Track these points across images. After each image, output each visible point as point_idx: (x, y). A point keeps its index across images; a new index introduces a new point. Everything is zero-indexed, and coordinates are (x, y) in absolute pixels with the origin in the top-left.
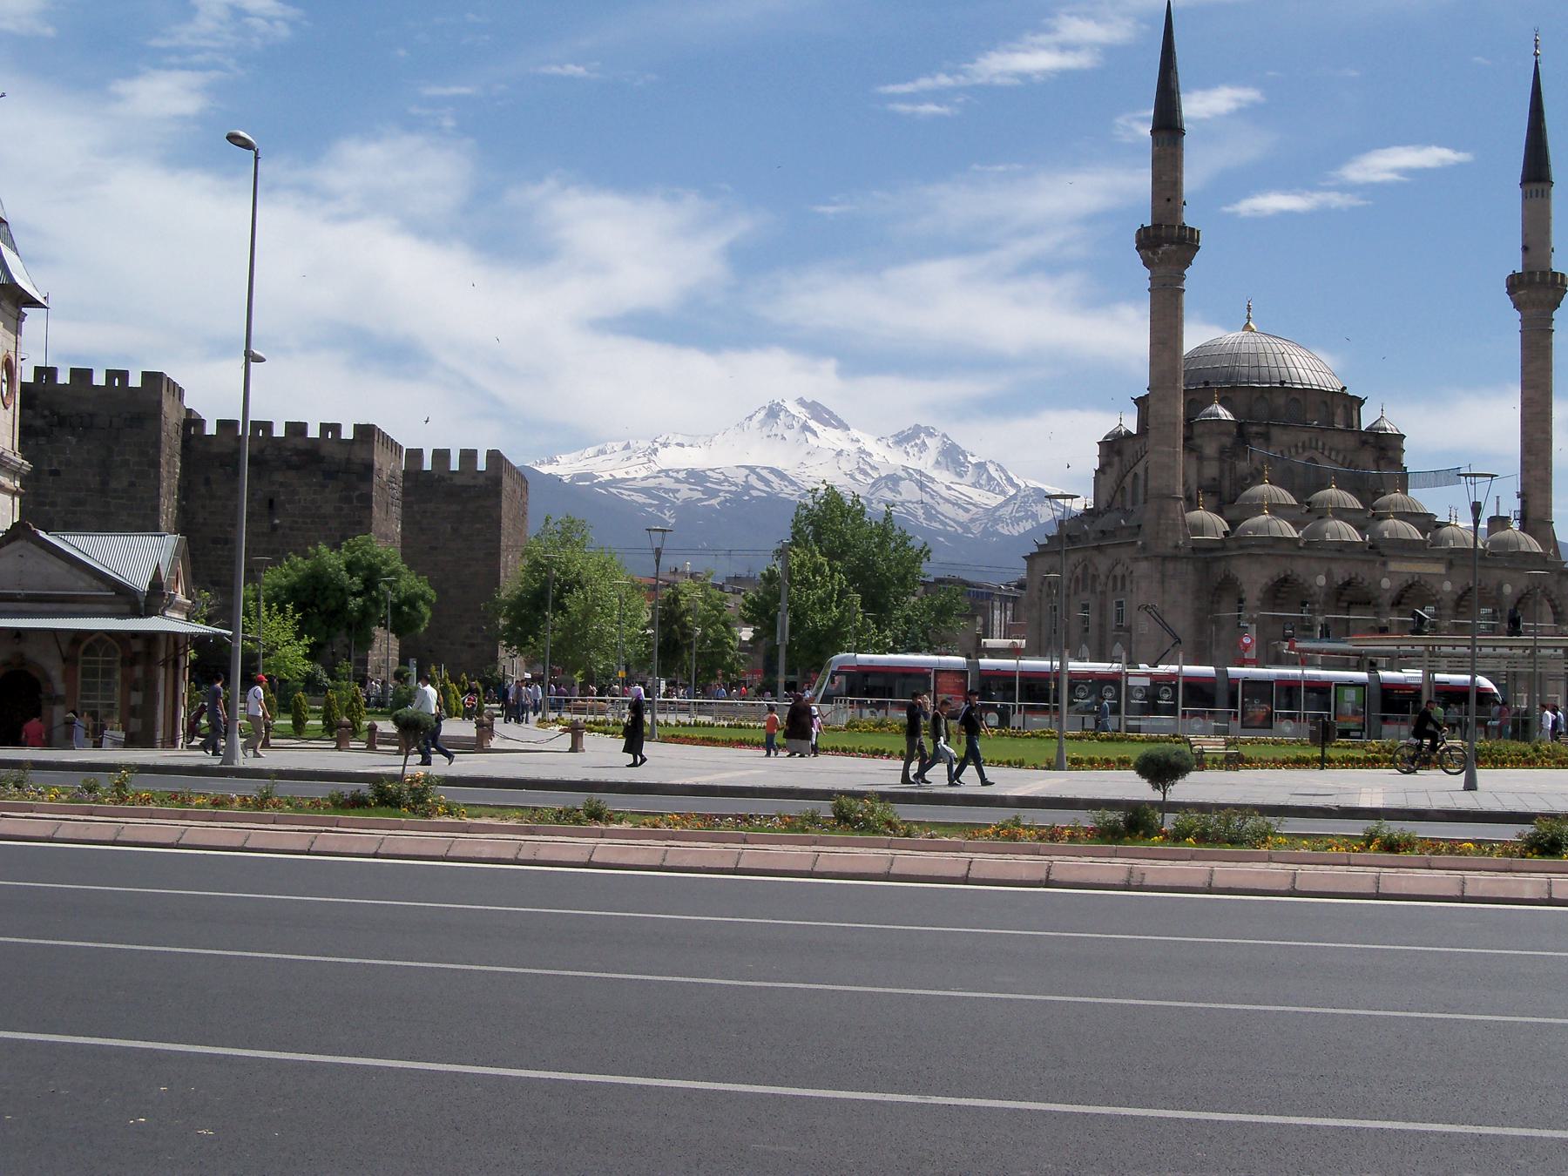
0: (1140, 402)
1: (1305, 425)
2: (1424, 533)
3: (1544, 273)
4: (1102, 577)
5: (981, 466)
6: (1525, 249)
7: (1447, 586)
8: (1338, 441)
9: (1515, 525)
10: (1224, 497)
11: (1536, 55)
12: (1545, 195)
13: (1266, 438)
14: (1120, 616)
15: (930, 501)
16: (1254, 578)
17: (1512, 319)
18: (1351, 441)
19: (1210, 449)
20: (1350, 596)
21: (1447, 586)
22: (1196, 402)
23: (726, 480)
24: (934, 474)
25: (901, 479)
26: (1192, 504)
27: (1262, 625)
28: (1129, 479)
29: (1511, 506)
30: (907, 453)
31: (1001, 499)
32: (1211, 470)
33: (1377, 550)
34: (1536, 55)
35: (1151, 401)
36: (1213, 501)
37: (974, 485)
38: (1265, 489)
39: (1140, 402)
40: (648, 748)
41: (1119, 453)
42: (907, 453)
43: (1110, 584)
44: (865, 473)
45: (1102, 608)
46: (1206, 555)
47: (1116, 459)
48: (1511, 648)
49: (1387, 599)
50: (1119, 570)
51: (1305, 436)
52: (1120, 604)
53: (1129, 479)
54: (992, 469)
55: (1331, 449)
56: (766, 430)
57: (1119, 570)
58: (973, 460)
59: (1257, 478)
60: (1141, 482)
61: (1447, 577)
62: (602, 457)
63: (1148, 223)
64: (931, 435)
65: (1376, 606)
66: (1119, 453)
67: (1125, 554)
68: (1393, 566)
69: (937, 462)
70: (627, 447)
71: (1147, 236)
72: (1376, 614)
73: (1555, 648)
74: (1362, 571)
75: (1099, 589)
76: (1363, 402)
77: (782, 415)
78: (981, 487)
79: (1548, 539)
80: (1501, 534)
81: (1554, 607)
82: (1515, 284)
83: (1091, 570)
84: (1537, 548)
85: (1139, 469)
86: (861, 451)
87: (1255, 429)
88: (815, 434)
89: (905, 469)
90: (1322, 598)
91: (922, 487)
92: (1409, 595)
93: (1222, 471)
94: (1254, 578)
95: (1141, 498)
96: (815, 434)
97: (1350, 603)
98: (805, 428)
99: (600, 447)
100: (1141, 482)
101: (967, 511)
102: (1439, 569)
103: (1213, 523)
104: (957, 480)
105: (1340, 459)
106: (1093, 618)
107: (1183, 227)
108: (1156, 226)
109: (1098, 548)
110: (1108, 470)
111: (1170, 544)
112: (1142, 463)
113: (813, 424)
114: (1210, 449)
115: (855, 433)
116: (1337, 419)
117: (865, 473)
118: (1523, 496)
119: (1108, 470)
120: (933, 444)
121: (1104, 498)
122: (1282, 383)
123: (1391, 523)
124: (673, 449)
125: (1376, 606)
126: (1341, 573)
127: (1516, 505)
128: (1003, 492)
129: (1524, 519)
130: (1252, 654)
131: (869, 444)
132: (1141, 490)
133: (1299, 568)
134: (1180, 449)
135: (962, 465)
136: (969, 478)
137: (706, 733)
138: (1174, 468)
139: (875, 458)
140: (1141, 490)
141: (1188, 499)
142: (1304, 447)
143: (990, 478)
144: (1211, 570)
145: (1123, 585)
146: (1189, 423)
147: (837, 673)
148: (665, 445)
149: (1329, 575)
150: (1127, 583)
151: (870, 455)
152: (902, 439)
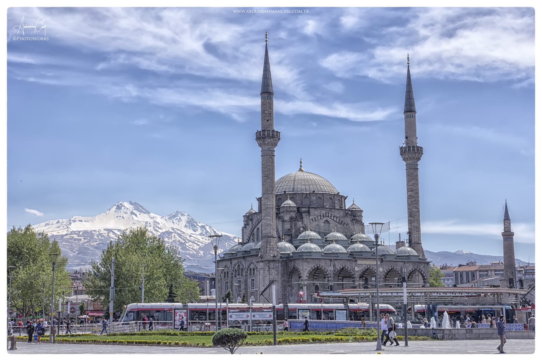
0: (259, 200)
1: (323, 207)
2: (371, 248)
3: (414, 147)
6: (407, 138)
7: (381, 269)
8: (336, 213)
9: (407, 245)
10: (292, 237)
11: (408, 63)
12: (413, 117)
13: (308, 212)
16: (305, 269)
17: (258, 150)
18: (342, 213)
19: (287, 218)
20: (344, 274)
21: (381, 269)
22: (280, 199)
24: (184, 230)
25: (172, 233)
26: (280, 239)
27: (308, 286)
28: (255, 230)
29: (405, 238)
30: (173, 222)
32: (287, 226)
33: (354, 256)
34: (266, 41)
35: (262, 199)
36: (288, 238)
37: (200, 234)
38: (308, 232)
39: (259, 200)
40: (409, 342)
41: (252, 220)
42: (173, 222)
44: (157, 231)
45: (246, 281)
46: (287, 261)
47: (250, 222)
48: (387, 293)
49: (357, 275)
50: (252, 266)
51: (324, 212)
54: (207, 228)
55: (334, 217)
56: (116, 214)
57: (252, 266)
58: (200, 225)
59: (305, 229)
60: (260, 231)
61: (381, 265)
62: (48, 226)
63: (260, 130)
64: (183, 215)
65: (354, 278)
66: (252, 220)
67: (254, 260)
68: (359, 262)
69: (186, 226)
70: (58, 222)
71: (260, 135)
72: (353, 281)
73: (421, 293)
74: (348, 265)
75: (244, 274)
76: (346, 198)
77: (123, 208)
78: (203, 235)
79: (420, 250)
80: (402, 248)
81: (423, 277)
83: (241, 267)
84: (415, 253)
85: (259, 226)
86: (155, 222)
87: (303, 209)
88: (136, 215)
89: (173, 229)
91: (180, 236)
92: (367, 275)
93: (291, 226)
94: (305, 269)
95: (260, 237)
96: (136, 215)
97: (343, 277)
98: (132, 213)
99: (47, 222)
100: (260, 231)
103: (287, 246)
104: (194, 233)
105: (338, 220)
106: (243, 286)
107: (273, 131)
108: (264, 131)
110: (248, 227)
111: (272, 255)
112: (260, 224)
113: (135, 211)
114: (287, 218)
115: (152, 215)
116: (336, 205)
117: (157, 231)
118: (410, 233)
119: (248, 227)
120: (184, 219)
121: (246, 238)
123: (356, 245)
124: (78, 223)
125: (354, 278)
126: (339, 266)
127: (407, 237)
129: (410, 242)
130: (305, 299)
131: (159, 219)
132: (260, 234)
133: (322, 264)
134: (275, 218)
135: (196, 227)
136: (199, 231)
137: (79, 339)
138: (271, 225)
139: (161, 224)
140: (260, 234)
141: (279, 237)
142: (323, 216)
143: (207, 232)
144: (288, 266)
146: (278, 208)
147: (130, 312)
148: (74, 221)
149: (334, 266)
150: (255, 271)
151: (158, 224)
152: (172, 217)
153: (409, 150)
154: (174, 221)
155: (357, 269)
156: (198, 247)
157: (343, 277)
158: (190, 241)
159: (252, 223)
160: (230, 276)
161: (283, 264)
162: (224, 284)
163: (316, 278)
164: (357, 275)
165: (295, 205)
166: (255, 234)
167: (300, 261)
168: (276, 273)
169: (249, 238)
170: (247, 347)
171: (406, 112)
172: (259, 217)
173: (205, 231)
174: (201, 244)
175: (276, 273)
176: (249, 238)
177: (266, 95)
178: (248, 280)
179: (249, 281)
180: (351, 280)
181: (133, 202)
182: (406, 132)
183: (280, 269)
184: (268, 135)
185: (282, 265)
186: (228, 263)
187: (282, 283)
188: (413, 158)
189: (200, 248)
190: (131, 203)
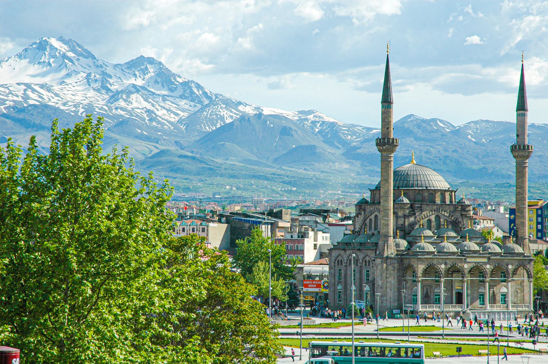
4: (361, 261)
5: (186, 84)
6: (518, 136)
11: (522, 61)
12: (524, 115)
14: (368, 275)
15: (152, 108)
23: (10, 93)
28: (368, 220)
30: (135, 75)
31: (199, 106)
43: (364, 263)
47: (363, 212)
52: (368, 271)
53: (368, 220)
58: (180, 80)
60: (373, 222)
68: (468, 260)
71: (380, 141)
75: (359, 265)
78: (186, 98)
82: (514, 149)
90: (443, 272)
100: (373, 222)
101: (176, 114)
102: (485, 260)
104: (171, 94)
108: (384, 139)
109: (359, 250)
122: (427, 187)
128: (200, 102)
132: (373, 225)
140: (373, 225)
145: (369, 265)
153: (520, 148)
154: (136, 73)
155: (466, 266)
156: (177, 118)
157: (453, 272)
158: (164, 108)
159: (365, 213)
160: (344, 264)
161: (399, 260)
162: (337, 271)
163: (428, 274)
164: (466, 271)
165: (408, 202)
166: (368, 224)
167: (415, 260)
168: (393, 269)
169: (361, 227)
170: (435, 360)
171: (518, 110)
172: (372, 209)
173: (188, 91)
174: (182, 114)
175: (393, 269)
176: (361, 227)
177: (386, 104)
178: (363, 271)
179: (364, 272)
180: (460, 275)
181: (67, 39)
182: (517, 130)
183: (396, 265)
184: (388, 142)
185: (398, 262)
186: (342, 252)
187: (398, 278)
188: (523, 156)
189: (180, 121)
190: (61, 39)
